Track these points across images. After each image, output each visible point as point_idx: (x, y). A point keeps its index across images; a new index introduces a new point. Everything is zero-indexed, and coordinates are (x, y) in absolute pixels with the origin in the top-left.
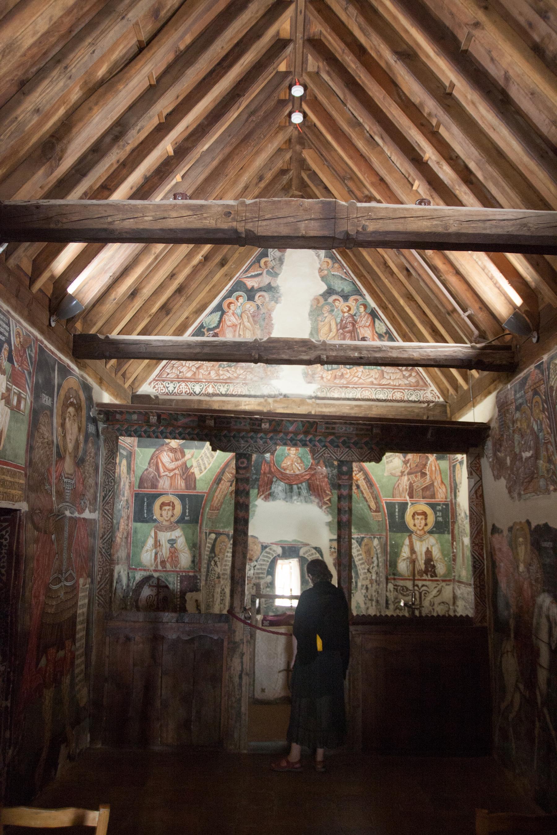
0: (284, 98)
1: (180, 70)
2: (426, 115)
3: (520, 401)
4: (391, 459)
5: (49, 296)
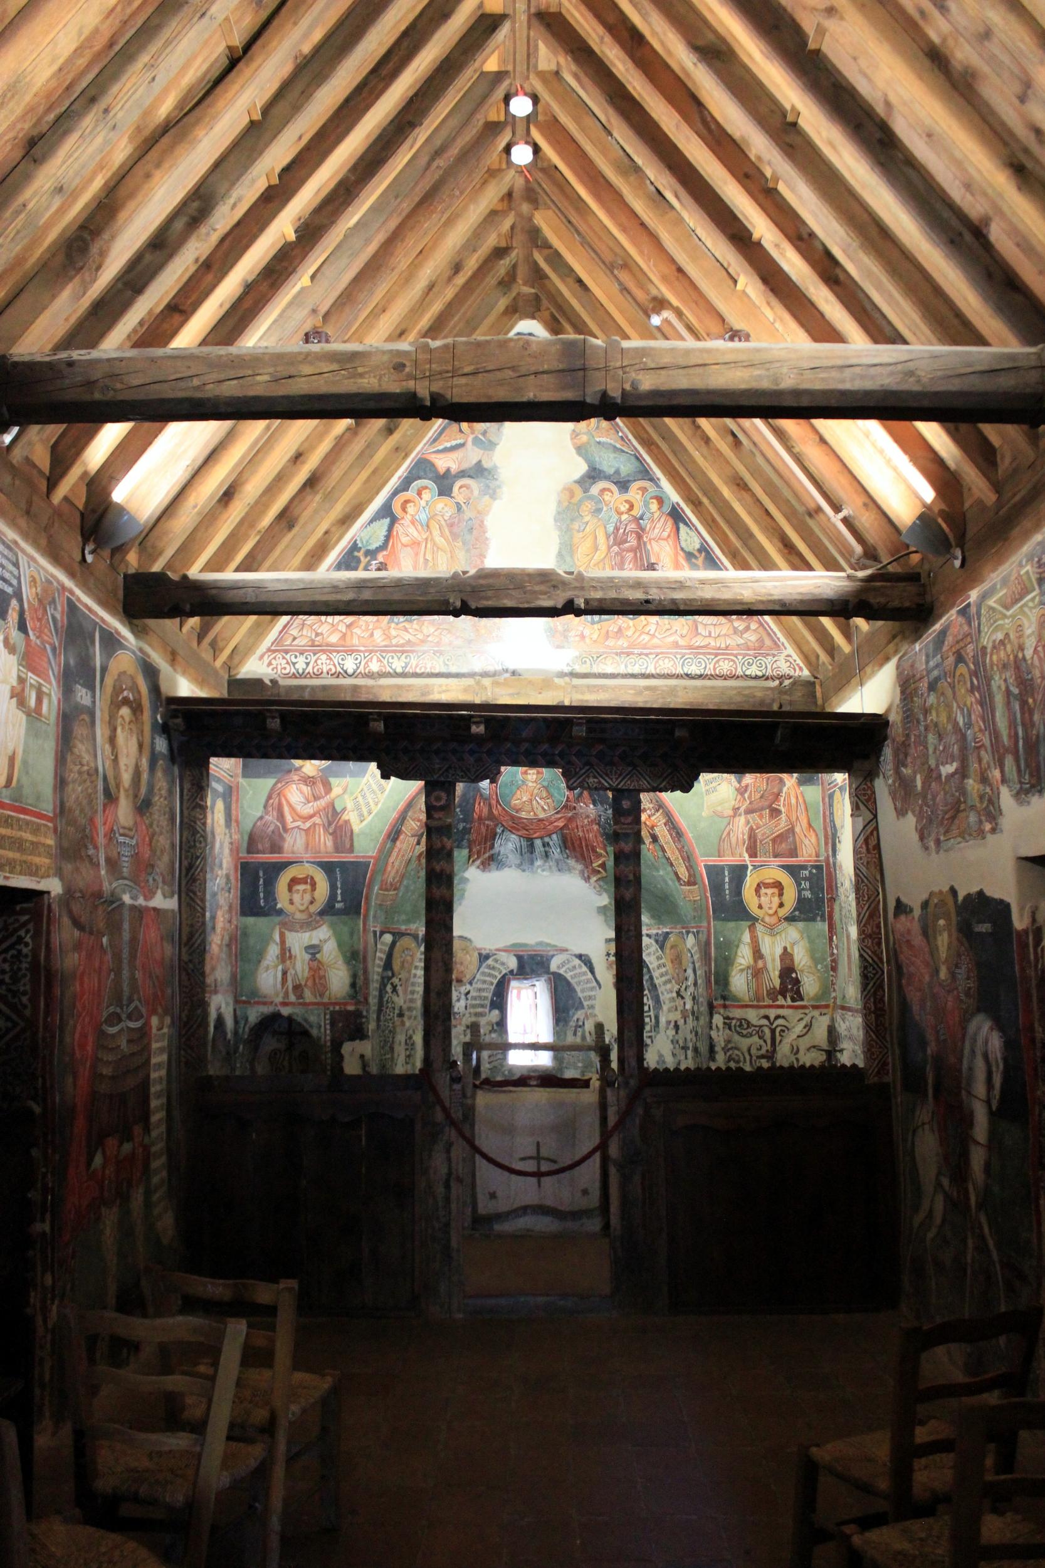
0: (496, 119)
1: (303, 92)
2: (753, 159)
3: (936, 673)
4: (714, 784)
5: (81, 507)
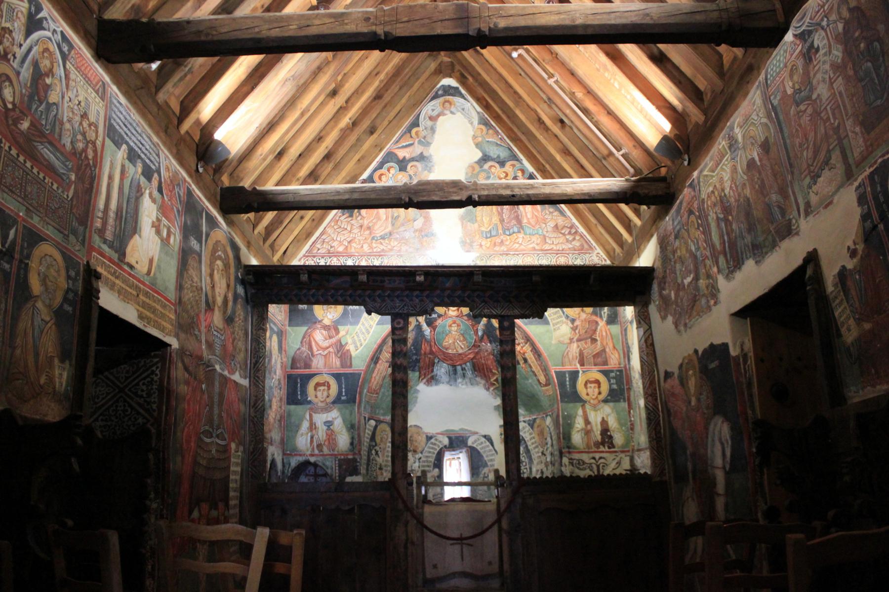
3: (678, 227)
